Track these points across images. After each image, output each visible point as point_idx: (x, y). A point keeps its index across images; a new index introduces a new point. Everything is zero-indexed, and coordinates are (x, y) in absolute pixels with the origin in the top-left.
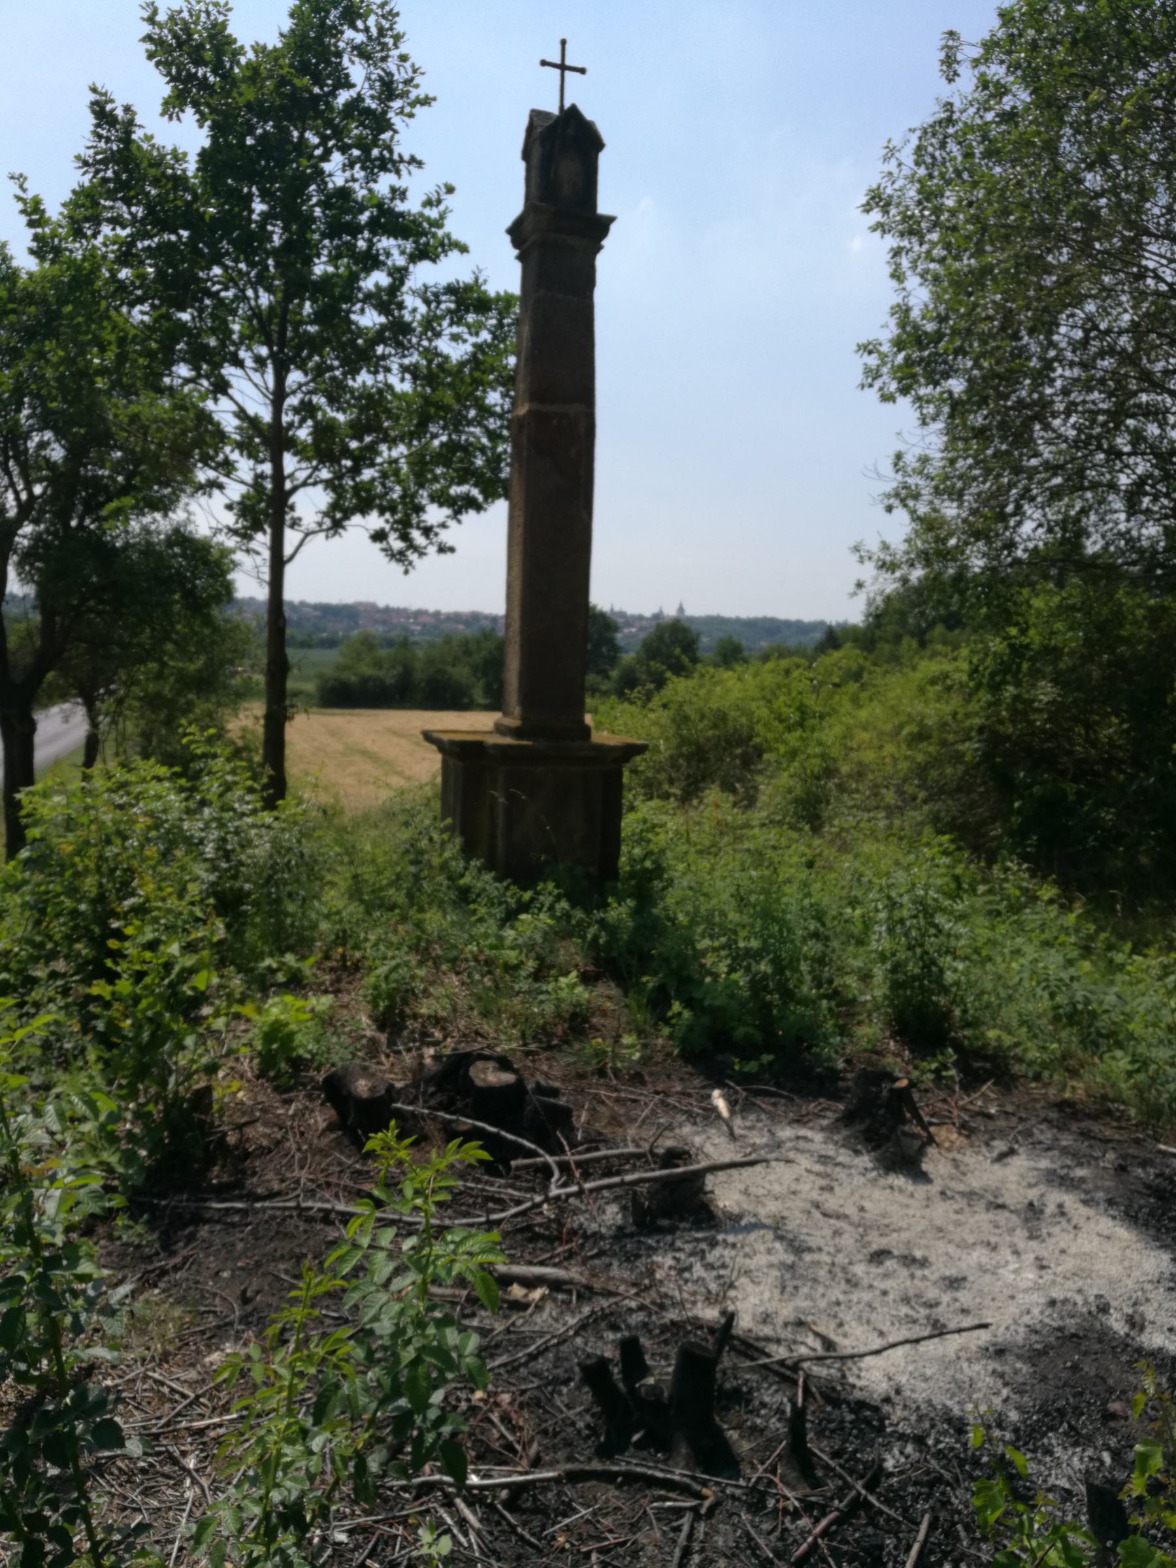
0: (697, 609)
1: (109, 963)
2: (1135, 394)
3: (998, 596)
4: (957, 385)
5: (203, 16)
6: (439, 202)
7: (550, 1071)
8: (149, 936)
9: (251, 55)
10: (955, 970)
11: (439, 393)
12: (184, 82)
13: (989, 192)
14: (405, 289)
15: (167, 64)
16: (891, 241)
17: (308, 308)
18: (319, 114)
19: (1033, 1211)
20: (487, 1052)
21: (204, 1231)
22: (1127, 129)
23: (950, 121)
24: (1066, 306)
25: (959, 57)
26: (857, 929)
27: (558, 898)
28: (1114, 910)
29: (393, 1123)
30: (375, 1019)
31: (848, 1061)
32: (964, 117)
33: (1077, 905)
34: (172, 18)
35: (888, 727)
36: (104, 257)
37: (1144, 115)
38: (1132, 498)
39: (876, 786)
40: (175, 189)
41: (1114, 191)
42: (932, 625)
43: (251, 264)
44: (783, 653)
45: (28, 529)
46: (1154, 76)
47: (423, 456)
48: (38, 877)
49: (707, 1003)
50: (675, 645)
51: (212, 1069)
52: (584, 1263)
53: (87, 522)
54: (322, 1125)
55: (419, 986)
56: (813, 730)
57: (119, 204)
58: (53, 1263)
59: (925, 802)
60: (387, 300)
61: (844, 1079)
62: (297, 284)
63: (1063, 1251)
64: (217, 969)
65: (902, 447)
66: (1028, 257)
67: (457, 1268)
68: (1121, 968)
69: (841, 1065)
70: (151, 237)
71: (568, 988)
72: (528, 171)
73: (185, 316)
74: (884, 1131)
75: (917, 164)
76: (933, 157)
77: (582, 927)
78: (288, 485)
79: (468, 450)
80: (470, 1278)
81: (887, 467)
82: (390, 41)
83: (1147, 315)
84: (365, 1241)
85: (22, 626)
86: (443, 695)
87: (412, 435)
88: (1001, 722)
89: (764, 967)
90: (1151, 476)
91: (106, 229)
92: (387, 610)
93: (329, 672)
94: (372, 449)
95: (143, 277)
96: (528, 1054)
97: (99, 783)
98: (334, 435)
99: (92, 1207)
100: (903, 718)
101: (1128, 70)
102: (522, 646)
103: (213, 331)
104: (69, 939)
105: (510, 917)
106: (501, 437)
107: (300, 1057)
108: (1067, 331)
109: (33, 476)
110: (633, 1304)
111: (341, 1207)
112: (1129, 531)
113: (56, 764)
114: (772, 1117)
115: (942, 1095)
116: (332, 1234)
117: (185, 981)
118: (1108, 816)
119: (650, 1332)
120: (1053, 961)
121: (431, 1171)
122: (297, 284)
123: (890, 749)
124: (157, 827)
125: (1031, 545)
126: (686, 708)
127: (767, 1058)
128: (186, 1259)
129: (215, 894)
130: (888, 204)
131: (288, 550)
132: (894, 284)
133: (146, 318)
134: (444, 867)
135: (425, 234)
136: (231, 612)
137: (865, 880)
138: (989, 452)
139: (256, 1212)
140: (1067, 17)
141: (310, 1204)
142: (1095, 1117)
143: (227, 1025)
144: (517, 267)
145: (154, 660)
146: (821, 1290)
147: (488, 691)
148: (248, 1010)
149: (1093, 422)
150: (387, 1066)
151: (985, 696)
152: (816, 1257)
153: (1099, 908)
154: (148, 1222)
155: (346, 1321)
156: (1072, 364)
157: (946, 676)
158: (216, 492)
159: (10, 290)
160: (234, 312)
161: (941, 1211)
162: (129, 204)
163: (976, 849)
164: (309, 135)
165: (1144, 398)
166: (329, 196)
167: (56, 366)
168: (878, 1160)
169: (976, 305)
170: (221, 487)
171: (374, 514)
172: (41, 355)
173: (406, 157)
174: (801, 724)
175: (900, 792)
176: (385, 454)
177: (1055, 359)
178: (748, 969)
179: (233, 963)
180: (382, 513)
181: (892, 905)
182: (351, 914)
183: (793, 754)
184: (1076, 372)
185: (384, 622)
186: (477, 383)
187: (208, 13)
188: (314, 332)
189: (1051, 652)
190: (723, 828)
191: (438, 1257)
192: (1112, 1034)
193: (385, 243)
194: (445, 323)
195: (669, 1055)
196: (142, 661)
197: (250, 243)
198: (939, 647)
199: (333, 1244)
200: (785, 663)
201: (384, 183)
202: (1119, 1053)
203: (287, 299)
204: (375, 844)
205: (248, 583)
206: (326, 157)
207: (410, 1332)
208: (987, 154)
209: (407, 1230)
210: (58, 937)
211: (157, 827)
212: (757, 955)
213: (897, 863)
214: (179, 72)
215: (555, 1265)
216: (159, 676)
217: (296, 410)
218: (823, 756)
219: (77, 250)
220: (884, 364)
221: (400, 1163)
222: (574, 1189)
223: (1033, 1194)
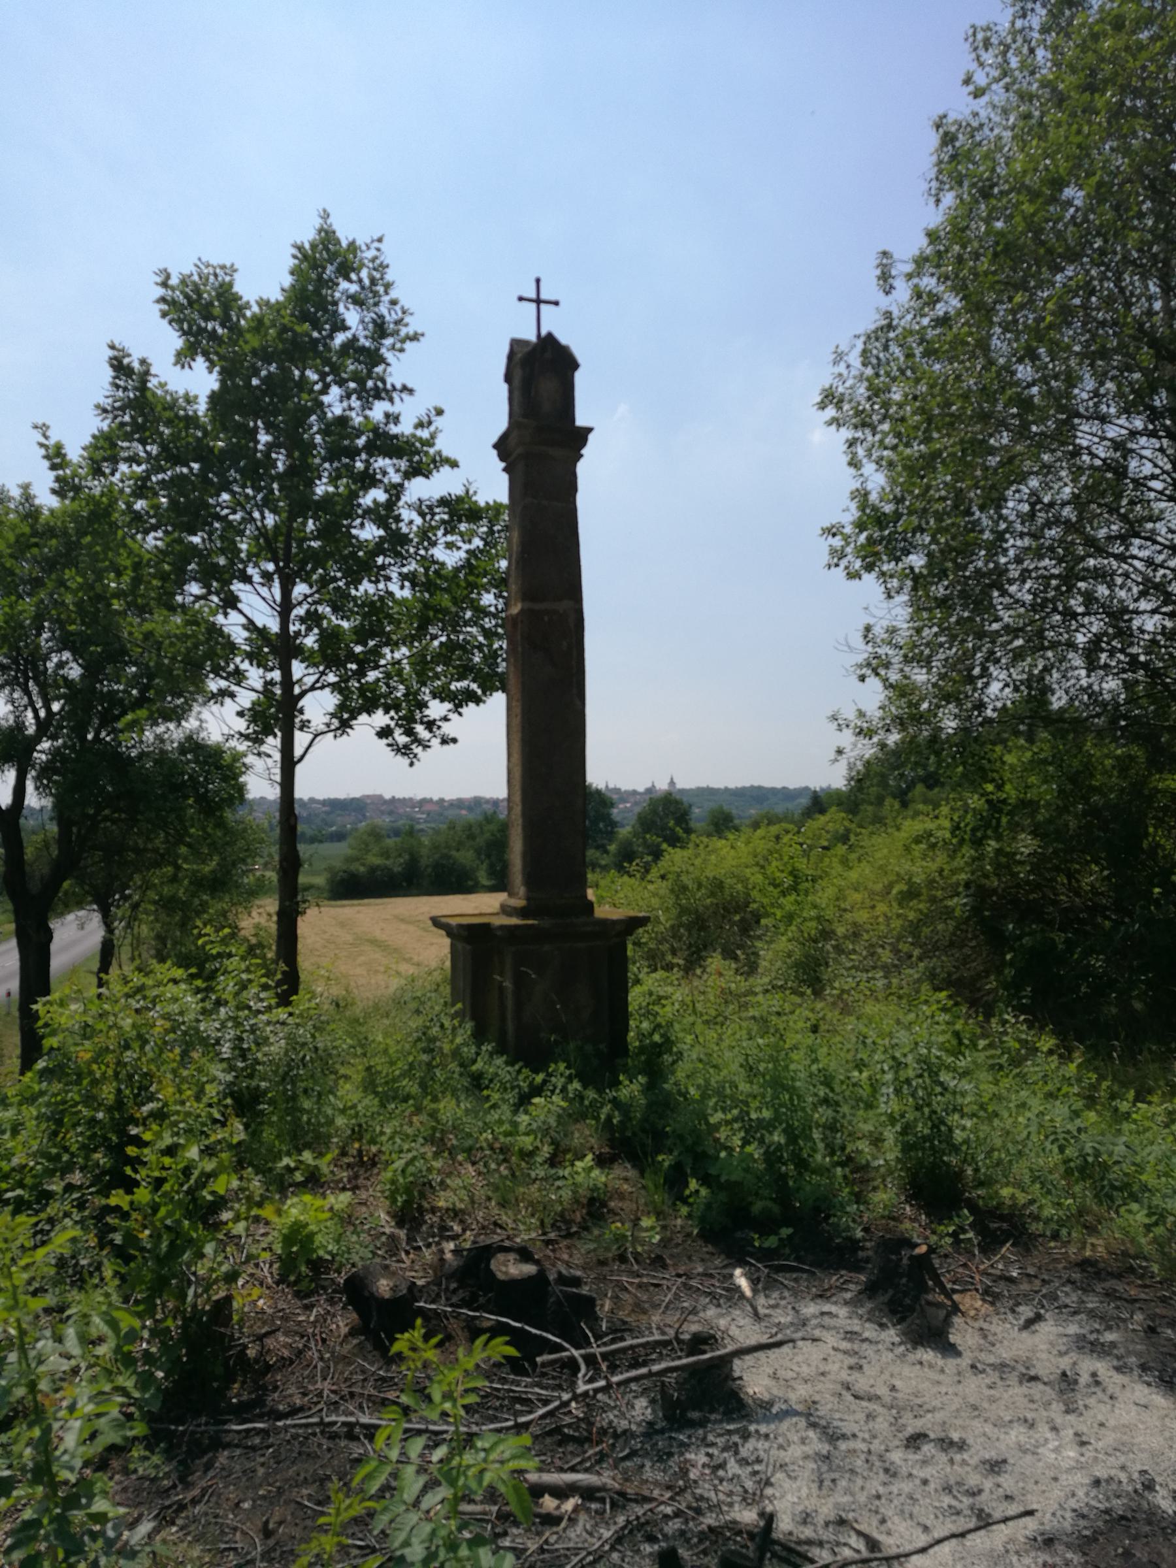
0: (687, 781)
1: (128, 1171)
2: (1083, 559)
3: (972, 755)
4: (917, 561)
5: (212, 278)
6: (430, 423)
7: (571, 1260)
8: (167, 1140)
9: (256, 309)
10: (964, 1128)
11: (437, 597)
12: (195, 336)
13: (932, 387)
14: (401, 503)
15: (180, 321)
16: (846, 433)
17: (311, 525)
18: (318, 354)
19: (1067, 1382)
20: (507, 1243)
21: (223, 1458)
22: (1050, 326)
23: (890, 327)
24: (1011, 483)
25: (894, 273)
26: (865, 1093)
27: (570, 1079)
28: (1111, 1057)
29: (419, 1322)
30: (393, 1215)
31: (866, 1230)
32: (902, 323)
33: (1076, 1054)
34: (183, 282)
35: (879, 887)
36: (122, 491)
37: (1065, 313)
38: (1091, 654)
39: (872, 946)
40: (187, 428)
41: (1044, 380)
42: (911, 785)
43: (257, 489)
44: (771, 820)
45: (46, 745)
46: (1071, 279)
47: (425, 656)
48: (57, 1086)
49: (723, 1179)
50: (669, 817)
51: (231, 1277)
52: (616, 1467)
53: (103, 734)
54: (344, 1330)
55: (436, 1178)
57: (135, 444)
58: (72, 1502)
59: (920, 959)
60: (384, 515)
61: (863, 1249)
62: (302, 505)
63: (1102, 1425)
64: (236, 1172)
65: (872, 621)
66: (973, 441)
67: (488, 1478)
68: (1127, 1116)
69: (859, 1234)
70: (164, 471)
71: (585, 1173)
72: (511, 392)
73: (196, 540)
74: (908, 1301)
75: (864, 365)
76: (878, 358)
77: (595, 1106)
78: (297, 690)
79: (465, 648)
80: (502, 1489)
81: (857, 641)
82: (381, 289)
83: (1085, 487)
84: (394, 1454)
85: (39, 838)
86: (449, 879)
87: (413, 638)
88: (986, 876)
89: (777, 1137)
90: (1106, 634)
91: (123, 467)
92: (393, 800)
93: (338, 864)
94: (376, 653)
95: (157, 507)
96: (548, 1243)
97: (117, 988)
98: (339, 641)
99: (111, 1437)
100: (893, 878)
101: (1046, 274)
102: (524, 828)
103: (222, 551)
104: (87, 1150)
105: (523, 1101)
106: (496, 634)
107: (320, 1258)
108: (1014, 505)
109: (52, 692)
110: (669, 1510)
111: (365, 1419)
112: (1090, 686)
113: (73, 971)
114: (795, 1293)
115: (963, 1260)
116: (357, 1450)
117: (204, 1186)
118: (1097, 963)
119: (688, 1541)
120: (1059, 1112)
121: (457, 1372)
122: (302, 505)
123: (882, 908)
124: (173, 1030)
125: (999, 705)
126: (684, 878)
127: (786, 1232)
128: (204, 1491)
129: (232, 1094)
130: (841, 401)
131: (298, 752)
132: (852, 471)
133: (159, 543)
134: (456, 1053)
135: (418, 453)
136: (242, 812)
137: (869, 1041)
138: (953, 619)
139: (277, 1430)
140: (988, 233)
141: (333, 1418)
142: (1119, 1276)
143: (247, 1229)
144: (505, 477)
145: (170, 863)
146: (860, 1482)
147: (492, 873)
148: (267, 1212)
149: (1047, 586)
150: (408, 1263)
151: (968, 852)
152: (851, 1444)
153: (1097, 1056)
154: (166, 1451)
155: (374, 1550)
156: (1022, 535)
157: (930, 834)
158: (228, 700)
159: (32, 526)
160: (241, 533)
161: (973, 1386)
162: (144, 443)
163: (973, 1003)
164: (308, 373)
165: (1092, 562)
166: (329, 425)
167: (74, 592)
168: (904, 1333)
169: (928, 487)
170: (232, 695)
171: (380, 712)
172: (62, 583)
173: (399, 386)
174: (794, 888)
175: (896, 951)
176: (389, 656)
177: (1006, 531)
178: (762, 1141)
179: (251, 1164)
180: (387, 712)
181: (898, 1065)
182: (366, 1108)
183: (790, 918)
184: (1027, 542)
185: (391, 813)
186: (472, 586)
187: (216, 275)
188: (318, 549)
189: (1027, 805)
190: (727, 996)
191: (469, 1467)
192: (1126, 1186)
193: (381, 462)
194: (440, 533)
195: (689, 1235)
196: (157, 865)
197: (256, 470)
198: (921, 807)
199: (358, 1461)
200: (774, 829)
201: (378, 411)
202: (1135, 1206)
203: (292, 518)
204: (386, 1034)
205: (260, 784)
206: (325, 390)
207: (442, 1554)
208: (927, 354)
209: (436, 1439)
210: (74, 1149)
211: (173, 1030)
212: (769, 1126)
213: (898, 1022)
214: (190, 327)
215: (586, 1470)
216: (174, 879)
217: (302, 620)
218: (819, 918)
219: (96, 487)
220: (848, 544)
221: (426, 1365)
222: (602, 1383)
223: (1065, 1363)
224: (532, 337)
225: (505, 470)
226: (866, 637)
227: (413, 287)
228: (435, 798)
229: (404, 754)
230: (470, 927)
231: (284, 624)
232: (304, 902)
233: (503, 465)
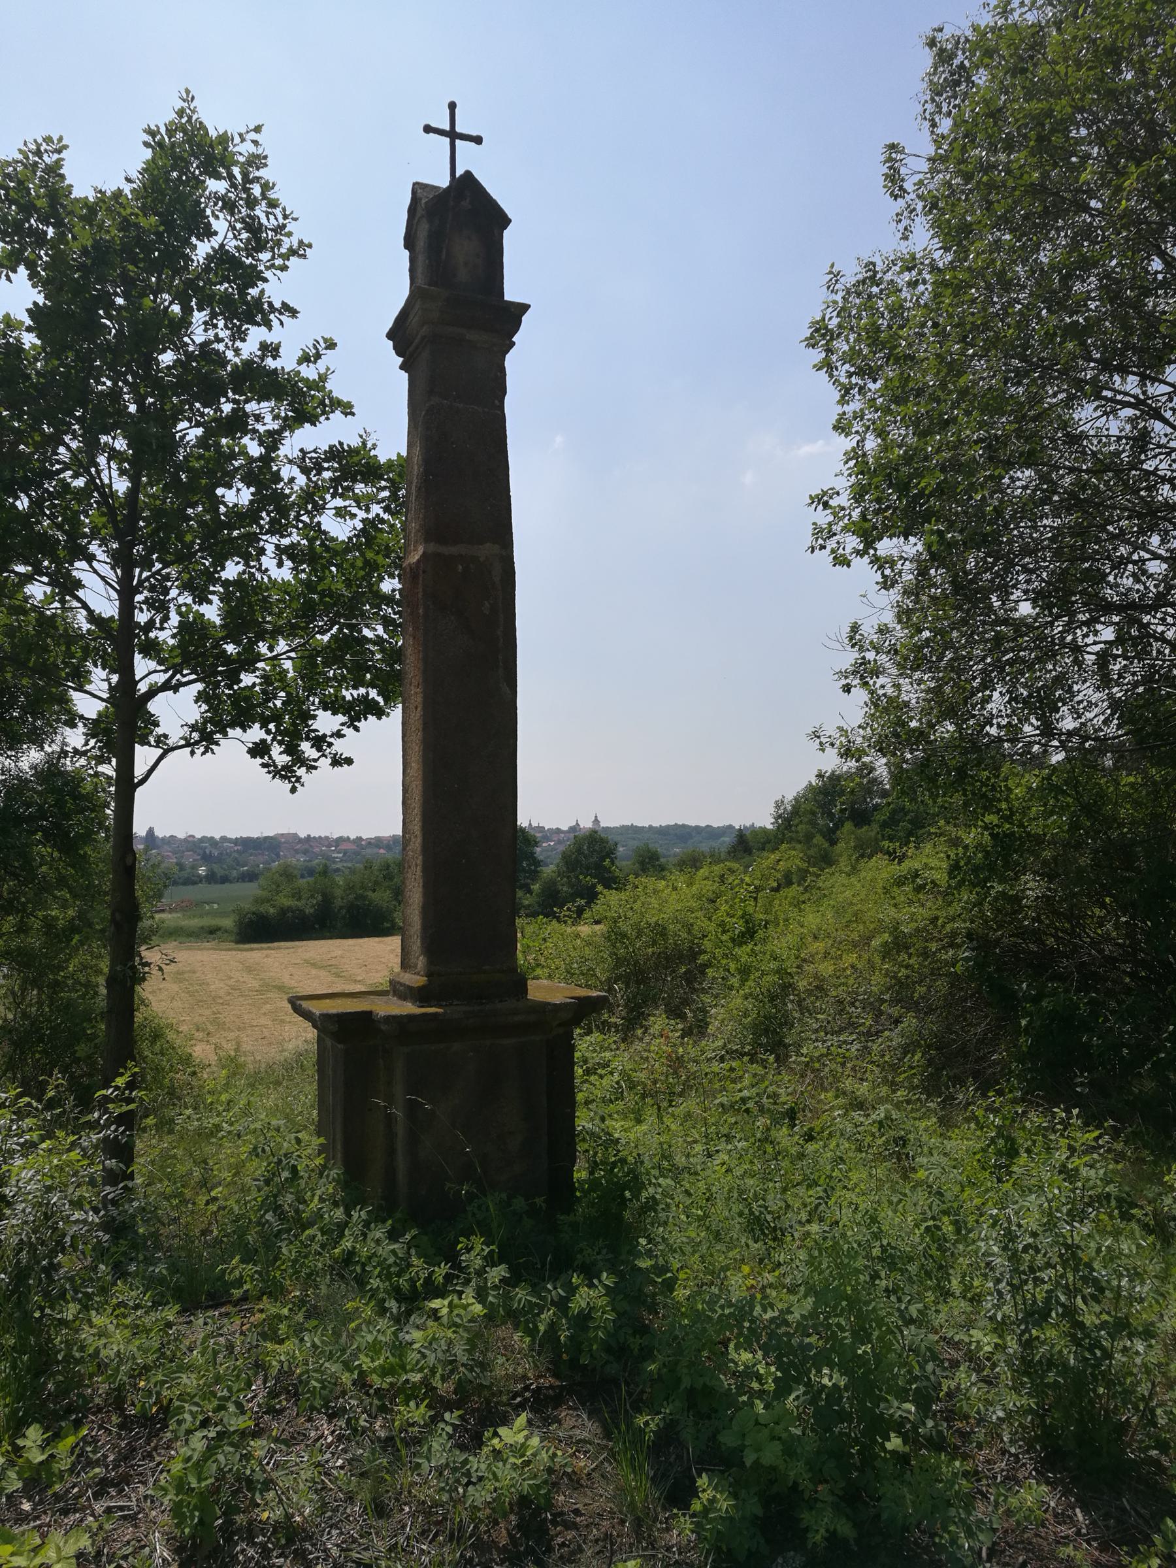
0: (610, 821)
6: (318, 356)
23: (873, 280)
42: (839, 825)
50: (596, 860)
56: (764, 941)
72: (412, 260)
78: (143, 687)
93: (247, 906)
102: (425, 869)
105: (412, 1300)
131: (139, 770)
173: (278, 305)
180: (264, 725)
183: (745, 972)
185: (305, 852)
224: (443, 182)
225: (402, 367)
226: (851, 638)
227: (295, 184)
228: (352, 837)
229: (283, 777)
233: (401, 360)
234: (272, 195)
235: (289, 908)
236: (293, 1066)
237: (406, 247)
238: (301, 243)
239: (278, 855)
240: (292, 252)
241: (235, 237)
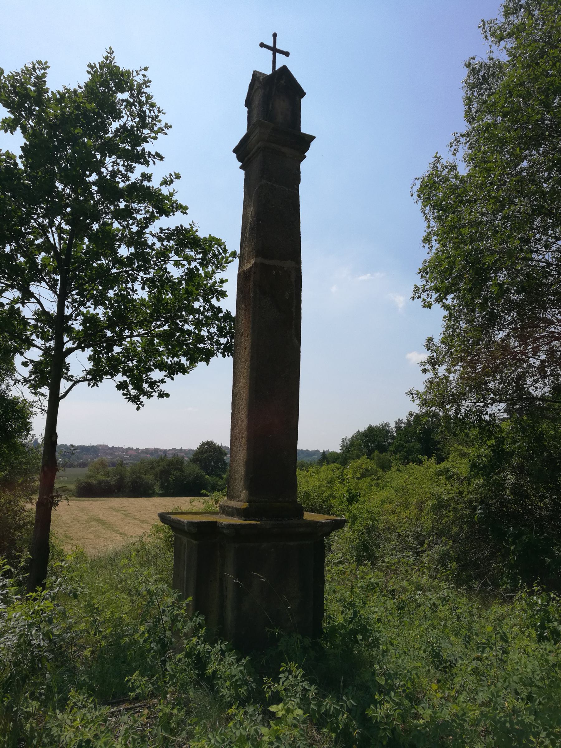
6: (171, 181)
72: (249, 113)
93: (83, 479)
102: (249, 440)
131: (62, 391)
157: (448, 470)
185: (111, 454)
205: (38, 425)
225: (241, 168)
226: (427, 346)
228: (134, 448)
229: (134, 401)
230: (199, 525)
231: (61, 307)
232: (58, 496)
233: (241, 164)
234: (153, 100)
235: (103, 481)
236: (144, 555)
237: (246, 105)
238: (166, 124)
239: (98, 455)
240: (161, 130)
241: (132, 120)
